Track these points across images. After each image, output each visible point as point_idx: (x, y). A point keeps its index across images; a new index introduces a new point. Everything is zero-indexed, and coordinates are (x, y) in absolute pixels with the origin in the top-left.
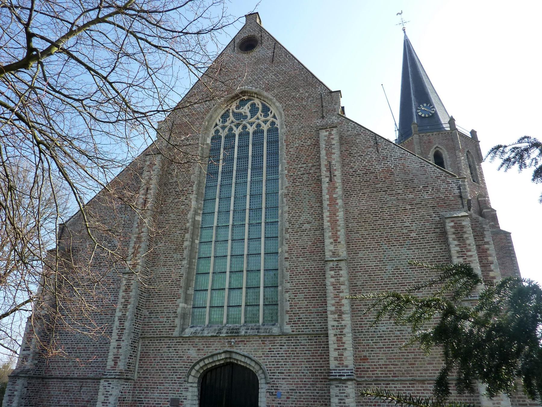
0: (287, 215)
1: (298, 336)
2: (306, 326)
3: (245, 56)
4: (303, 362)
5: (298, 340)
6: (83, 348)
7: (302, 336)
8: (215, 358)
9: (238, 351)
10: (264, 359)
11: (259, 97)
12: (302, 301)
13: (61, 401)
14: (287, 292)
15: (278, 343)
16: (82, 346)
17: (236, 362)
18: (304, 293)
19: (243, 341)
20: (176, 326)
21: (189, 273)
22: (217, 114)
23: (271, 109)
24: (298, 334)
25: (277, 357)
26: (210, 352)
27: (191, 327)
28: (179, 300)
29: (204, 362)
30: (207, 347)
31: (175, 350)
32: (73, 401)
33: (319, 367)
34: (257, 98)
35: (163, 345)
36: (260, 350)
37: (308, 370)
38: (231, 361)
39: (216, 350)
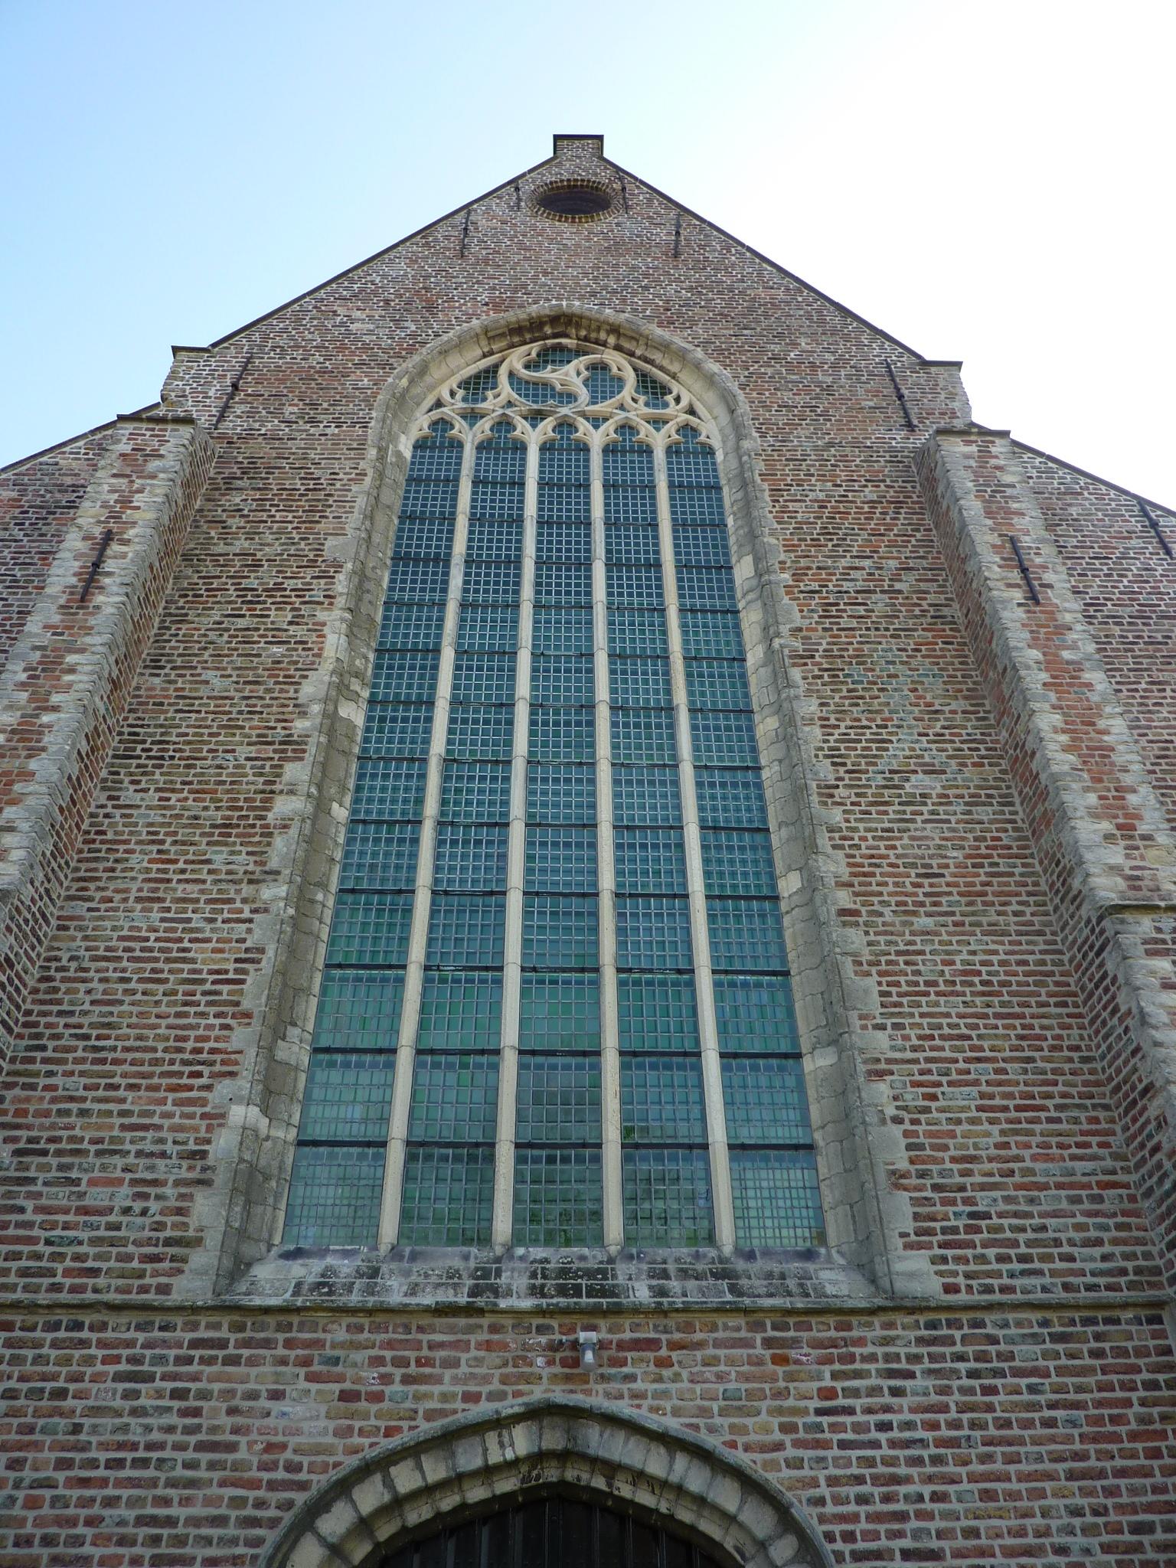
0: (818, 732)
1: (989, 1318)
2: (1023, 1258)
3: (565, 227)
4: (1050, 1476)
5: (993, 1340)
7: (1011, 1316)
8: (469, 1458)
9: (624, 1408)
10: (796, 1464)
11: (626, 345)
12: (973, 1121)
14: (881, 1074)
15: (872, 1358)
17: (599, 1483)
18: (976, 1083)
19: (652, 1344)
20: (198, 1242)
21: (293, 951)
22: (444, 369)
23: (676, 388)
24: (990, 1307)
25: (875, 1445)
26: (430, 1416)
27: (288, 1256)
28: (224, 1088)
29: (388, 1483)
30: (407, 1380)
31: (176, 1394)
33: (1150, 1508)
34: (618, 348)
35: (89, 1361)
36: (764, 1405)
37: (1088, 1530)
38: (570, 1475)
39: (471, 1398)
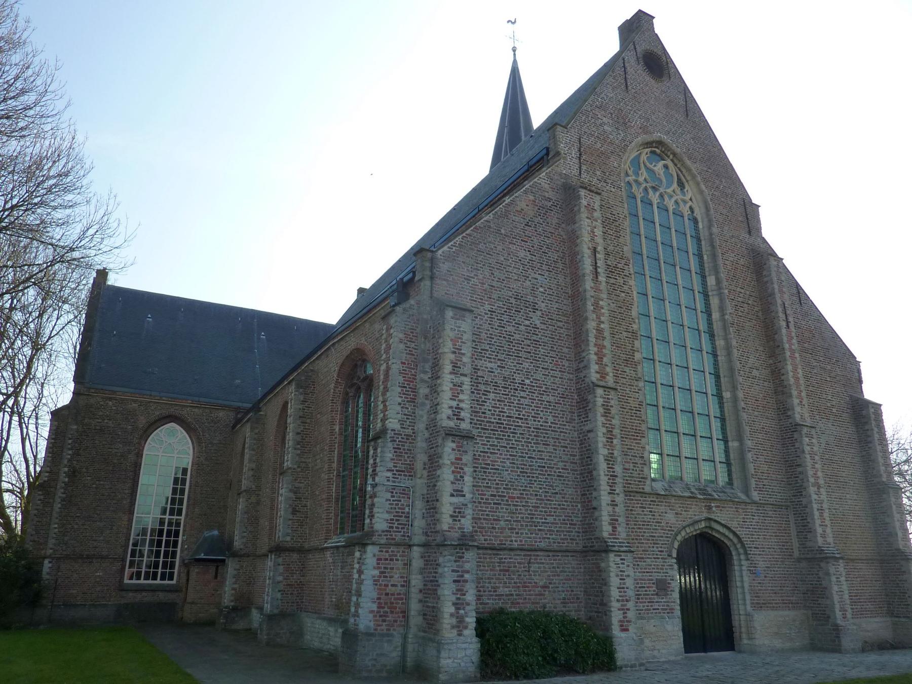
3: (648, 78)
6: (518, 498)
13: (499, 588)
16: (516, 494)
32: (519, 587)
34: (672, 160)
